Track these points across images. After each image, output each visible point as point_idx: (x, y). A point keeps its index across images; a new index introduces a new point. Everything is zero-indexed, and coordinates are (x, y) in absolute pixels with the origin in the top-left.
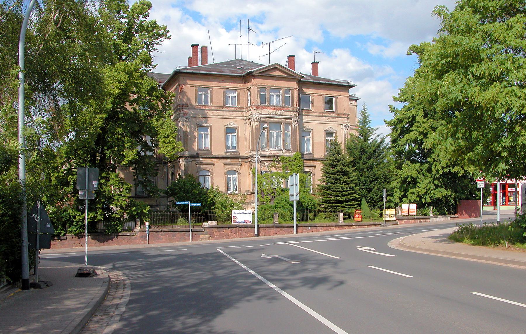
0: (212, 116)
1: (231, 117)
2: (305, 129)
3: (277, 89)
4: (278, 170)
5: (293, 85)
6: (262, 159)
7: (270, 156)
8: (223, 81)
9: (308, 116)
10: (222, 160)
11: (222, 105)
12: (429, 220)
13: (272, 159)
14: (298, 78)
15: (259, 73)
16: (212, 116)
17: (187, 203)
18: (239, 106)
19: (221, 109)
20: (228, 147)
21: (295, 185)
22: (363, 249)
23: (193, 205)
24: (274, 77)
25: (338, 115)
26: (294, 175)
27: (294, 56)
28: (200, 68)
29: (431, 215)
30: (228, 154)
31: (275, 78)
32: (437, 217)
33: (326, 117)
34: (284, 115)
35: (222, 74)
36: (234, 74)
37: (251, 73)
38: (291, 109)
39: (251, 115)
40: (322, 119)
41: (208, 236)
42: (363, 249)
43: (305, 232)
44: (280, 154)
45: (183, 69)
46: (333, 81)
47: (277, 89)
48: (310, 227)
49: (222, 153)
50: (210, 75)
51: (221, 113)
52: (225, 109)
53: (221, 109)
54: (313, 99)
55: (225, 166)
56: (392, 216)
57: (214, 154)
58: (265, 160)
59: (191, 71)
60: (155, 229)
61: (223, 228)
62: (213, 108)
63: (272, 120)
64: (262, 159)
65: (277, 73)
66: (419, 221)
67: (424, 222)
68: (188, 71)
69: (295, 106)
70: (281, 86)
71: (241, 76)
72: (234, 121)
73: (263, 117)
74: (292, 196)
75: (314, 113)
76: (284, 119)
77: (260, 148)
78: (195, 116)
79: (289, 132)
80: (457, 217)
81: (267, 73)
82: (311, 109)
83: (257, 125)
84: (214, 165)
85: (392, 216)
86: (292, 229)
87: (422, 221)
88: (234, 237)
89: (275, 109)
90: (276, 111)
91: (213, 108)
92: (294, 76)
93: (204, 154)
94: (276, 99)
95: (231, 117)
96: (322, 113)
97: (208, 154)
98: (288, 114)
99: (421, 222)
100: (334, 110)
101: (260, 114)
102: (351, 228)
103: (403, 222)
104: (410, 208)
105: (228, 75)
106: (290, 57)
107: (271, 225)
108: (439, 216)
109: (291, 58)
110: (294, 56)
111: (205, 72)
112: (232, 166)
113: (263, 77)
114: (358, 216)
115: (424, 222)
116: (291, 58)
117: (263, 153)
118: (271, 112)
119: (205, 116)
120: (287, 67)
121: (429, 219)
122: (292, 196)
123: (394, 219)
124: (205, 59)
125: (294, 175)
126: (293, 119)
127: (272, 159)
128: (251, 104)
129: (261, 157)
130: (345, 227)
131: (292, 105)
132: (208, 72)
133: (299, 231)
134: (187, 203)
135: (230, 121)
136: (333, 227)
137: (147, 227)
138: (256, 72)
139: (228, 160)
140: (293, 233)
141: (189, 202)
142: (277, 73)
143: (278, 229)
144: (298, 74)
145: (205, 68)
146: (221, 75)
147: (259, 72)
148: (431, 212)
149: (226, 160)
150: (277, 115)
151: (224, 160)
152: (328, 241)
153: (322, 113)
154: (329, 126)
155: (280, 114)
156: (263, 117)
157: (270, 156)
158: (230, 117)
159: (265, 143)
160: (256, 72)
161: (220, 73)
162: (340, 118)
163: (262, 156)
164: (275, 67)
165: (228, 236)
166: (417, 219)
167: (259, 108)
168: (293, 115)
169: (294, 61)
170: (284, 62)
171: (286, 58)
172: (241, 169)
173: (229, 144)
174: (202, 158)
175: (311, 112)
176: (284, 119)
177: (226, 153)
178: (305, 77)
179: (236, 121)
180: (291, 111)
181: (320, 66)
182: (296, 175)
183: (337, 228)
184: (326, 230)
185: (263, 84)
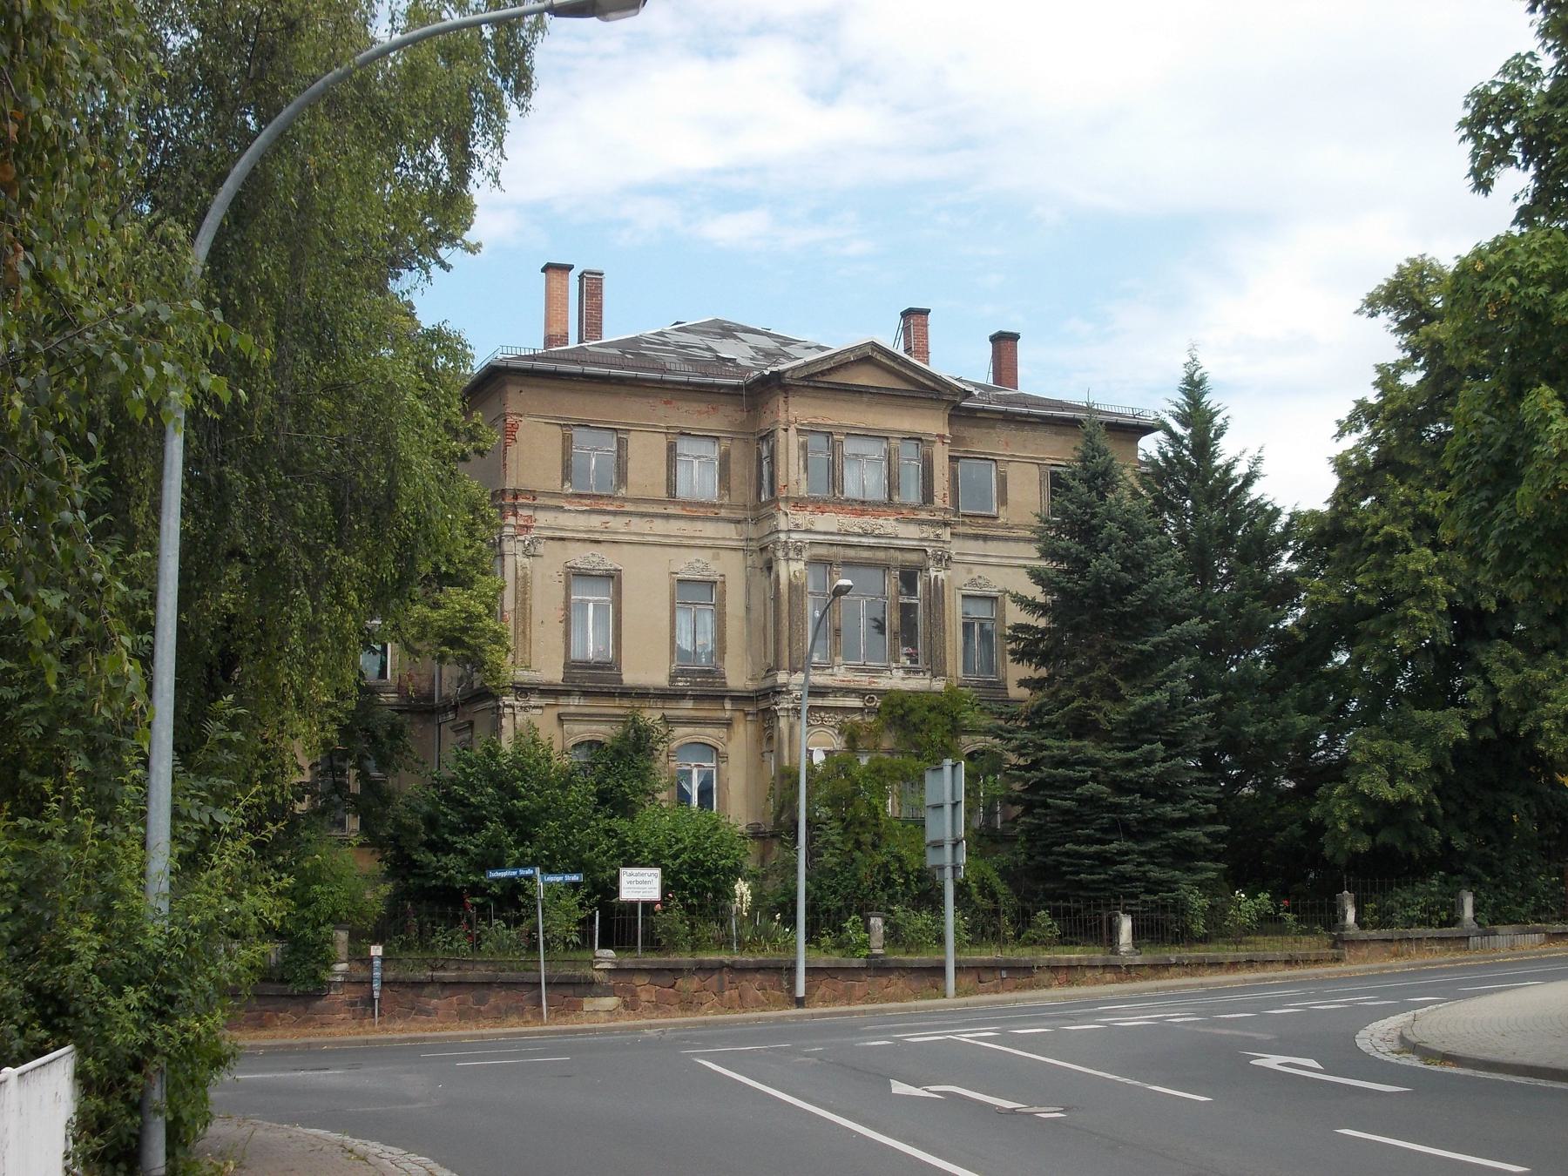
5: (933, 424)
11: (663, 494)
14: (951, 398)
17: (529, 872)
18: (726, 500)
20: (684, 654)
21: (948, 808)
22: (1272, 1061)
23: (551, 879)
26: (947, 770)
27: (927, 312)
28: (577, 356)
30: (681, 683)
34: (896, 537)
35: (667, 377)
36: (710, 380)
37: (778, 375)
38: (924, 515)
39: (771, 533)
42: (1272, 1061)
45: (520, 358)
46: (1061, 405)
50: (621, 381)
51: (659, 526)
57: (630, 677)
59: (550, 366)
62: (629, 507)
65: (864, 377)
68: (539, 365)
69: (938, 502)
70: (882, 427)
71: (737, 388)
72: (705, 555)
74: (939, 845)
75: (1006, 527)
82: (994, 512)
89: (862, 513)
90: (867, 522)
91: (629, 507)
92: (934, 389)
94: (862, 479)
101: (808, 531)
105: (688, 383)
106: (908, 314)
109: (914, 318)
110: (927, 312)
111: (604, 371)
116: (914, 318)
117: (819, 679)
120: (900, 351)
122: (939, 845)
124: (591, 322)
125: (947, 770)
127: (855, 702)
128: (772, 492)
131: (928, 495)
132: (614, 372)
134: (529, 872)
135: (692, 556)
137: (377, 963)
141: (538, 870)
142: (864, 377)
144: (949, 385)
145: (604, 355)
146: (662, 381)
152: (1110, 1028)
157: (847, 691)
158: (692, 542)
161: (657, 376)
163: (817, 691)
164: (870, 356)
167: (803, 508)
168: (932, 537)
169: (926, 333)
170: (890, 338)
171: (896, 321)
172: (729, 739)
173: (685, 642)
175: (998, 526)
177: (673, 678)
178: (976, 393)
179: (716, 557)
180: (922, 522)
181: (1024, 351)
182: (954, 767)
185: (819, 421)
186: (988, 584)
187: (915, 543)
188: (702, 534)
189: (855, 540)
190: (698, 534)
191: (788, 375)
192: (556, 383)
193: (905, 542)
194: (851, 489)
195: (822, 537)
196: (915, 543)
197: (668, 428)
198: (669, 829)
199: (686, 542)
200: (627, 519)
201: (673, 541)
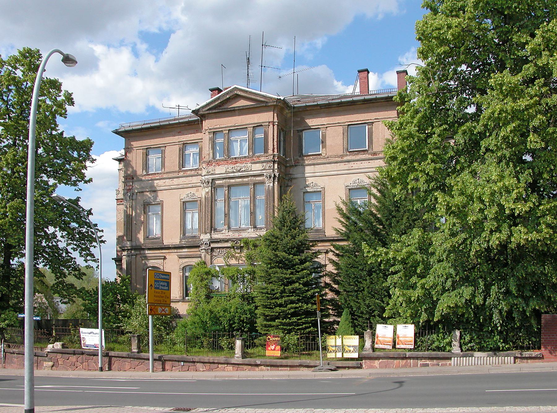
0: (164, 187)
1: (190, 185)
2: (308, 189)
3: (242, 128)
4: (240, 262)
6: (213, 245)
7: (227, 241)
8: (180, 133)
9: (314, 165)
10: (176, 251)
12: (448, 362)
13: (229, 244)
15: (208, 110)
16: (164, 187)
19: (176, 175)
24: (234, 110)
25: (375, 154)
29: (456, 349)
31: (237, 112)
32: (472, 356)
33: (349, 161)
34: (251, 171)
38: (263, 159)
40: (342, 166)
41: (51, 363)
43: (175, 370)
44: (244, 235)
47: (242, 128)
48: (184, 362)
49: (176, 241)
52: (181, 174)
53: (176, 175)
54: (324, 136)
55: (180, 260)
56: (352, 349)
57: (166, 242)
58: (220, 248)
60: (11, 350)
61: (68, 354)
62: (165, 176)
63: (232, 181)
64: (213, 245)
65: (242, 103)
66: (420, 362)
67: (433, 365)
69: (270, 152)
72: (193, 190)
73: (219, 179)
76: (252, 176)
77: (212, 228)
78: (140, 190)
79: (261, 197)
80: (541, 358)
81: (225, 106)
83: (208, 193)
84: (165, 258)
85: (352, 349)
86: (147, 362)
87: (428, 362)
88: (80, 369)
89: (236, 162)
91: (165, 176)
93: (152, 243)
95: (190, 185)
96: (342, 156)
97: (155, 243)
98: (259, 167)
99: (427, 365)
100: (367, 148)
102: (257, 369)
103: (377, 363)
104: (398, 332)
107: (125, 354)
108: (477, 354)
112: (190, 260)
113: (218, 115)
114: (273, 347)
115: (433, 365)
117: (216, 236)
118: (230, 168)
119: (153, 189)
121: (450, 359)
123: (356, 355)
126: (265, 174)
127: (229, 244)
129: (213, 242)
130: (245, 367)
131: (266, 151)
133: (167, 367)
136: (223, 366)
138: (204, 110)
139: (184, 250)
140: (148, 370)
142: (242, 103)
143: (137, 362)
147: (207, 109)
148: (456, 344)
149: (181, 251)
150: (239, 171)
151: (179, 251)
153: (342, 156)
154: (354, 177)
155: (243, 169)
156: (219, 179)
157: (227, 241)
159: (220, 219)
160: (204, 110)
162: (377, 159)
165: (74, 366)
166: (413, 358)
174: (149, 249)
176: (252, 176)
177: (181, 240)
179: (197, 191)
180: (262, 162)
183: (230, 368)
184: (210, 370)
186: (316, 185)
187: (259, 172)
188: (192, 182)
189: (232, 175)
190: (190, 182)
191: (200, 110)
192: (147, 133)
193: (255, 172)
194: (237, 153)
195: (218, 176)
196: (259, 172)
197: (179, 142)
198: (244, 285)
199: (185, 186)
200: (164, 181)
201: (180, 186)
